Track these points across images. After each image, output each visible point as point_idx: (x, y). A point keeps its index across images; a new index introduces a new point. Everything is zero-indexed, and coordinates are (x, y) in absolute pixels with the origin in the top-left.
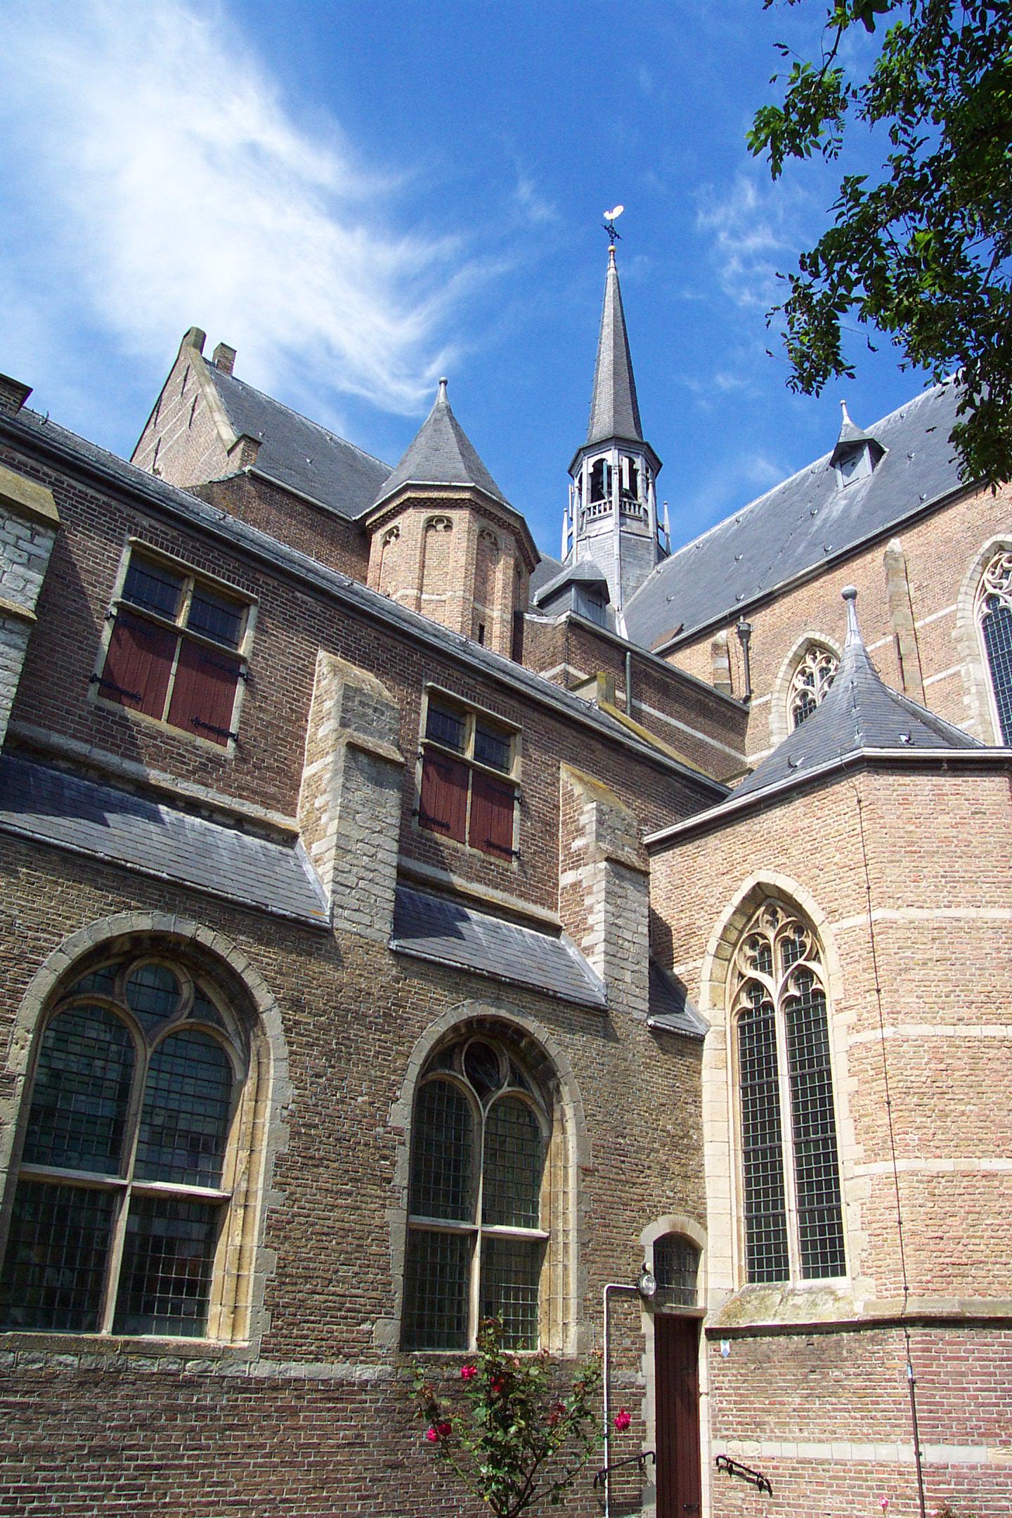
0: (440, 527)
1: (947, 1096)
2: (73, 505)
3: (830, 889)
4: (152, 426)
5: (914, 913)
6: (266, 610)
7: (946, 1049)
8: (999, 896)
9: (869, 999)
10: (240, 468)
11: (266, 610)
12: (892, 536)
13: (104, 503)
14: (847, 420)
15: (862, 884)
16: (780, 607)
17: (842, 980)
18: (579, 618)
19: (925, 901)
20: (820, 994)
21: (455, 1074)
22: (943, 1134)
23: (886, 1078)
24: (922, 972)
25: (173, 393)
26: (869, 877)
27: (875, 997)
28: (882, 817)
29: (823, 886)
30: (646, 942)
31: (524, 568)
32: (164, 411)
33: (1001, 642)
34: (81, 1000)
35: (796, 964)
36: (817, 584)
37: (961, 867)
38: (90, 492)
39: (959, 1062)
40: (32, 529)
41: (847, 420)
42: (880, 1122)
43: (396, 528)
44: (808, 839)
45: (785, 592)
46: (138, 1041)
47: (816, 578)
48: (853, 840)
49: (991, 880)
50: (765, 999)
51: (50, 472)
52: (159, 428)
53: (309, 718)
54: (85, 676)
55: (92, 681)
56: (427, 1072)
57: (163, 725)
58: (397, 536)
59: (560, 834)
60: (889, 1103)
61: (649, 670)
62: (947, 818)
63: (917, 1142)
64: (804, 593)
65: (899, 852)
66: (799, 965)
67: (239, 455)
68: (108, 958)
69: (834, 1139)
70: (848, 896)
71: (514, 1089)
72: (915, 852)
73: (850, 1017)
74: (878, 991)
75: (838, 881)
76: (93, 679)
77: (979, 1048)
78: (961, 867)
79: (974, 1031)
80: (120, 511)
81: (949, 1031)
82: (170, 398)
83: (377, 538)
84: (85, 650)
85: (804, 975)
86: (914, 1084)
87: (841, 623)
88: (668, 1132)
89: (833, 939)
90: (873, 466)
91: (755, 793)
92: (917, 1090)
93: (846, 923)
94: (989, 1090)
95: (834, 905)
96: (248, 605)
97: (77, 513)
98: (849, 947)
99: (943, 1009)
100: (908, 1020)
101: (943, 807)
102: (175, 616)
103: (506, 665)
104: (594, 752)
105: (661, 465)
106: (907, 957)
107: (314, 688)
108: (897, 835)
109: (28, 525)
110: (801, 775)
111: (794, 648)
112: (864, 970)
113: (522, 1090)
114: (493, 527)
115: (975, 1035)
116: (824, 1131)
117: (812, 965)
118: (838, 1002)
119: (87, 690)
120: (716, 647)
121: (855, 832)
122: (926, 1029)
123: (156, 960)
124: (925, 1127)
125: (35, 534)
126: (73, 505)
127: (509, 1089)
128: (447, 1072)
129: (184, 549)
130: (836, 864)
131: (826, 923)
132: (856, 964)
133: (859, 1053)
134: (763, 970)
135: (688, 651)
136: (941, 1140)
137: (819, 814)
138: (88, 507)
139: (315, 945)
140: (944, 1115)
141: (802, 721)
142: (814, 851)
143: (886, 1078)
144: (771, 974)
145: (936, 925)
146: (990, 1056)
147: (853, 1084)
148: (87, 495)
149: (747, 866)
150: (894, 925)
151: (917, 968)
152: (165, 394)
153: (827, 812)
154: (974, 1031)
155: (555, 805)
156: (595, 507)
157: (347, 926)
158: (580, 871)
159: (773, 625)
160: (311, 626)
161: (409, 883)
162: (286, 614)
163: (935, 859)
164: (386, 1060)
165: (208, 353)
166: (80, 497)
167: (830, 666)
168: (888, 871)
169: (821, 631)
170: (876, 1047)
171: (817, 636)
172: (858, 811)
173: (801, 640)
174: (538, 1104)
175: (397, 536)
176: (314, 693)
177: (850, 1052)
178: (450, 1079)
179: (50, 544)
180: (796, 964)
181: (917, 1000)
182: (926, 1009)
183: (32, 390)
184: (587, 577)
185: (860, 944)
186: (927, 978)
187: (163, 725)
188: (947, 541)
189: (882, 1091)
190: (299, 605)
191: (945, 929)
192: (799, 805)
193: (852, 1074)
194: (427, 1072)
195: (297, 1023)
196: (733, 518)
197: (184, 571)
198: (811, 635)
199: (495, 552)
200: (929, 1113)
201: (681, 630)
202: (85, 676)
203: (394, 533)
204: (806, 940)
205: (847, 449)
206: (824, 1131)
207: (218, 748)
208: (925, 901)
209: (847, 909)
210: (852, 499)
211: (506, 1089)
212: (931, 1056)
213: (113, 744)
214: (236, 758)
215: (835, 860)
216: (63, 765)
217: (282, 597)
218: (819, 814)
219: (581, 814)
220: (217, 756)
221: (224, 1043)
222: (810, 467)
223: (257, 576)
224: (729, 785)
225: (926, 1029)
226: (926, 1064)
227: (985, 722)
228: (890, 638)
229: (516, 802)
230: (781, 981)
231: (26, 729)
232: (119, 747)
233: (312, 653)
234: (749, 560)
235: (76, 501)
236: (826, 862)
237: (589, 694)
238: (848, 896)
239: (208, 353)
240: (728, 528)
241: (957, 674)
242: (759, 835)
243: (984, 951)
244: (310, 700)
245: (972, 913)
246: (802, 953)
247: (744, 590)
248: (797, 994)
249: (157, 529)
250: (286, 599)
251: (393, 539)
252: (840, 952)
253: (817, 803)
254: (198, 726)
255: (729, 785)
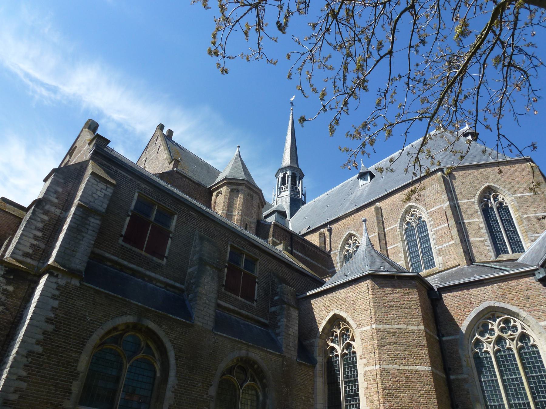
0: (235, 191)
1: (398, 391)
2: (120, 179)
3: (358, 317)
4: (145, 153)
5: (386, 326)
6: (180, 217)
7: (397, 374)
8: (414, 322)
9: (371, 355)
10: (172, 169)
11: (180, 217)
12: (377, 202)
13: (130, 179)
14: (363, 165)
15: (369, 316)
16: (340, 223)
17: (362, 349)
18: (278, 223)
19: (390, 323)
20: (354, 353)
21: (232, 377)
22: (397, 404)
23: (377, 383)
24: (389, 347)
25: (152, 143)
26: (372, 314)
27: (373, 355)
28: (376, 294)
29: (356, 316)
30: (297, 332)
31: (261, 207)
32: (149, 149)
33: (411, 237)
34: (106, 346)
35: (347, 342)
36: (353, 216)
37: (401, 311)
38: (126, 175)
39: (402, 378)
40: (106, 186)
41: (363, 165)
42: (375, 399)
43: (221, 191)
44: (351, 300)
45: (343, 218)
46: (125, 361)
47: (353, 214)
48: (366, 301)
49: (411, 316)
50: (336, 354)
51: (114, 168)
52: (147, 153)
53: (191, 253)
54: (119, 235)
55: (121, 237)
56: (222, 375)
57: (143, 253)
58: (221, 194)
59: (270, 294)
60: (378, 392)
61: (299, 241)
62: (397, 295)
63: (388, 407)
64: (349, 218)
65: (381, 306)
66: (348, 342)
67: (173, 165)
68: (117, 332)
69: (359, 404)
70: (364, 320)
71: (251, 382)
72: (386, 306)
73: (365, 361)
74: (374, 353)
75: (361, 315)
76: (121, 236)
77: (408, 373)
78: (401, 311)
79: (406, 367)
80: (135, 182)
81: (398, 367)
82: (151, 145)
83: (214, 194)
84: (120, 226)
85: (349, 346)
86: (387, 386)
87: (360, 228)
88: (303, 399)
89: (359, 334)
90: (371, 180)
91: (334, 284)
92: (388, 388)
93: (364, 329)
94: (412, 389)
95: (360, 323)
96: (174, 215)
97: (121, 181)
98: (365, 337)
99: (396, 360)
100: (384, 363)
101: (395, 291)
102: (150, 217)
103: (254, 237)
104: (282, 267)
105: (304, 176)
106: (384, 341)
107: (194, 243)
108: (380, 300)
109: (105, 185)
110: (350, 278)
111: (345, 236)
112: (370, 345)
113: (254, 383)
114: (252, 193)
115: (407, 369)
116: (356, 401)
117: (352, 343)
118: (361, 356)
119: (119, 239)
120: (320, 234)
121: (367, 298)
122: (390, 366)
123: (133, 333)
124: (391, 401)
125: (107, 187)
126: (120, 179)
127: (250, 382)
128: (229, 375)
129: (155, 195)
130: (360, 309)
131: (357, 329)
132: (366, 343)
133: (367, 374)
134: (335, 343)
135: (311, 235)
136: (396, 406)
137: (355, 292)
138: (125, 180)
139: (188, 330)
140: (397, 397)
141: (349, 260)
142: (353, 304)
143: (377, 383)
144: (338, 345)
145: (393, 331)
146: (412, 377)
147: (366, 385)
148: (125, 176)
149: (330, 308)
150: (380, 330)
151: (387, 345)
152: (150, 143)
153: (358, 291)
154: (406, 367)
155: (269, 285)
156: (283, 187)
157: (199, 324)
158: (276, 307)
159: (338, 228)
160: (194, 223)
161: (220, 309)
162: (186, 218)
163: (393, 309)
164: (209, 371)
165: (165, 131)
166: (123, 177)
167: (356, 242)
168: (377, 312)
169: (354, 230)
170: (374, 372)
171: (353, 232)
172: (368, 291)
173: (347, 233)
174: (258, 387)
175: (221, 194)
176: (193, 245)
177: (365, 373)
178: (230, 378)
179: (112, 191)
180: (347, 342)
181: (387, 356)
182: (390, 360)
183: (110, 141)
184: (280, 210)
185: (368, 336)
186: (391, 349)
187: (143, 253)
188: (394, 204)
189: (376, 388)
190: (190, 215)
191: (396, 332)
192: (348, 289)
193: (365, 381)
194: (222, 375)
195: (180, 357)
196: (326, 193)
197: (155, 203)
198: (350, 232)
199: (252, 201)
200: (392, 396)
201: (309, 228)
202: (119, 235)
203: (220, 193)
204: (350, 334)
205: (363, 174)
206: (356, 401)
207: (160, 261)
208: (390, 323)
209: (364, 324)
210: (364, 189)
211: (248, 382)
212: (392, 376)
213: (126, 258)
214: (166, 264)
215: (360, 307)
216: (109, 264)
217: (185, 213)
218: (355, 292)
219: (278, 288)
220: (160, 264)
221: (154, 363)
222: (351, 179)
223: (178, 205)
224: (324, 280)
225: (390, 366)
226: (391, 379)
227: (406, 262)
228: (376, 234)
229: (256, 283)
230: (342, 348)
231: (97, 251)
232: (128, 259)
233: (193, 231)
234: (331, 207)
235: (122, 178)
236: (357, 308)
237: (280, 248)
238: (364, 320)
239: (165, 131)
240: (324, 197)
241: (397, 246)
242: (335, 298)
243: (409, 340)
244: (192, 247)
245: (405, 327)
246: (349, 338)
247: (330, 216)
248: (347, 352)
249: (147, 188)
250: (187, 214)
251: (220, 194)
252: (361, 338)
253: (354, 288)
254: (154, 253)
255: (324, 280)
